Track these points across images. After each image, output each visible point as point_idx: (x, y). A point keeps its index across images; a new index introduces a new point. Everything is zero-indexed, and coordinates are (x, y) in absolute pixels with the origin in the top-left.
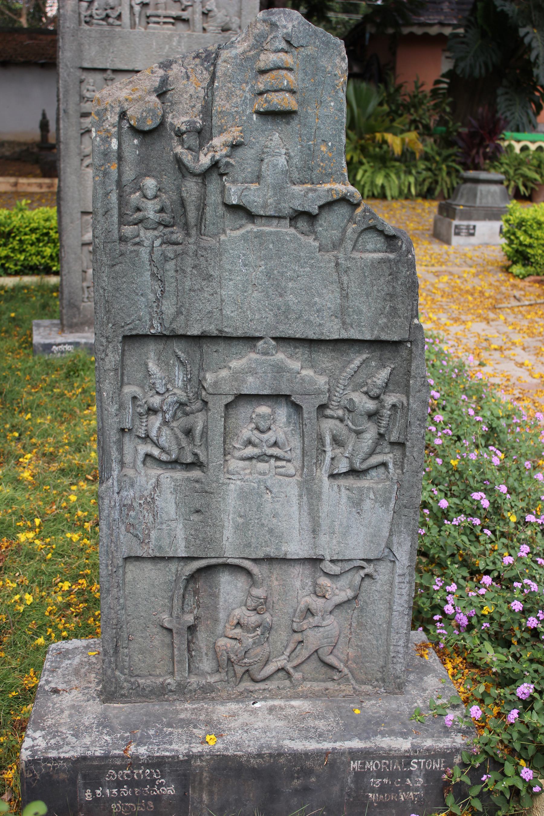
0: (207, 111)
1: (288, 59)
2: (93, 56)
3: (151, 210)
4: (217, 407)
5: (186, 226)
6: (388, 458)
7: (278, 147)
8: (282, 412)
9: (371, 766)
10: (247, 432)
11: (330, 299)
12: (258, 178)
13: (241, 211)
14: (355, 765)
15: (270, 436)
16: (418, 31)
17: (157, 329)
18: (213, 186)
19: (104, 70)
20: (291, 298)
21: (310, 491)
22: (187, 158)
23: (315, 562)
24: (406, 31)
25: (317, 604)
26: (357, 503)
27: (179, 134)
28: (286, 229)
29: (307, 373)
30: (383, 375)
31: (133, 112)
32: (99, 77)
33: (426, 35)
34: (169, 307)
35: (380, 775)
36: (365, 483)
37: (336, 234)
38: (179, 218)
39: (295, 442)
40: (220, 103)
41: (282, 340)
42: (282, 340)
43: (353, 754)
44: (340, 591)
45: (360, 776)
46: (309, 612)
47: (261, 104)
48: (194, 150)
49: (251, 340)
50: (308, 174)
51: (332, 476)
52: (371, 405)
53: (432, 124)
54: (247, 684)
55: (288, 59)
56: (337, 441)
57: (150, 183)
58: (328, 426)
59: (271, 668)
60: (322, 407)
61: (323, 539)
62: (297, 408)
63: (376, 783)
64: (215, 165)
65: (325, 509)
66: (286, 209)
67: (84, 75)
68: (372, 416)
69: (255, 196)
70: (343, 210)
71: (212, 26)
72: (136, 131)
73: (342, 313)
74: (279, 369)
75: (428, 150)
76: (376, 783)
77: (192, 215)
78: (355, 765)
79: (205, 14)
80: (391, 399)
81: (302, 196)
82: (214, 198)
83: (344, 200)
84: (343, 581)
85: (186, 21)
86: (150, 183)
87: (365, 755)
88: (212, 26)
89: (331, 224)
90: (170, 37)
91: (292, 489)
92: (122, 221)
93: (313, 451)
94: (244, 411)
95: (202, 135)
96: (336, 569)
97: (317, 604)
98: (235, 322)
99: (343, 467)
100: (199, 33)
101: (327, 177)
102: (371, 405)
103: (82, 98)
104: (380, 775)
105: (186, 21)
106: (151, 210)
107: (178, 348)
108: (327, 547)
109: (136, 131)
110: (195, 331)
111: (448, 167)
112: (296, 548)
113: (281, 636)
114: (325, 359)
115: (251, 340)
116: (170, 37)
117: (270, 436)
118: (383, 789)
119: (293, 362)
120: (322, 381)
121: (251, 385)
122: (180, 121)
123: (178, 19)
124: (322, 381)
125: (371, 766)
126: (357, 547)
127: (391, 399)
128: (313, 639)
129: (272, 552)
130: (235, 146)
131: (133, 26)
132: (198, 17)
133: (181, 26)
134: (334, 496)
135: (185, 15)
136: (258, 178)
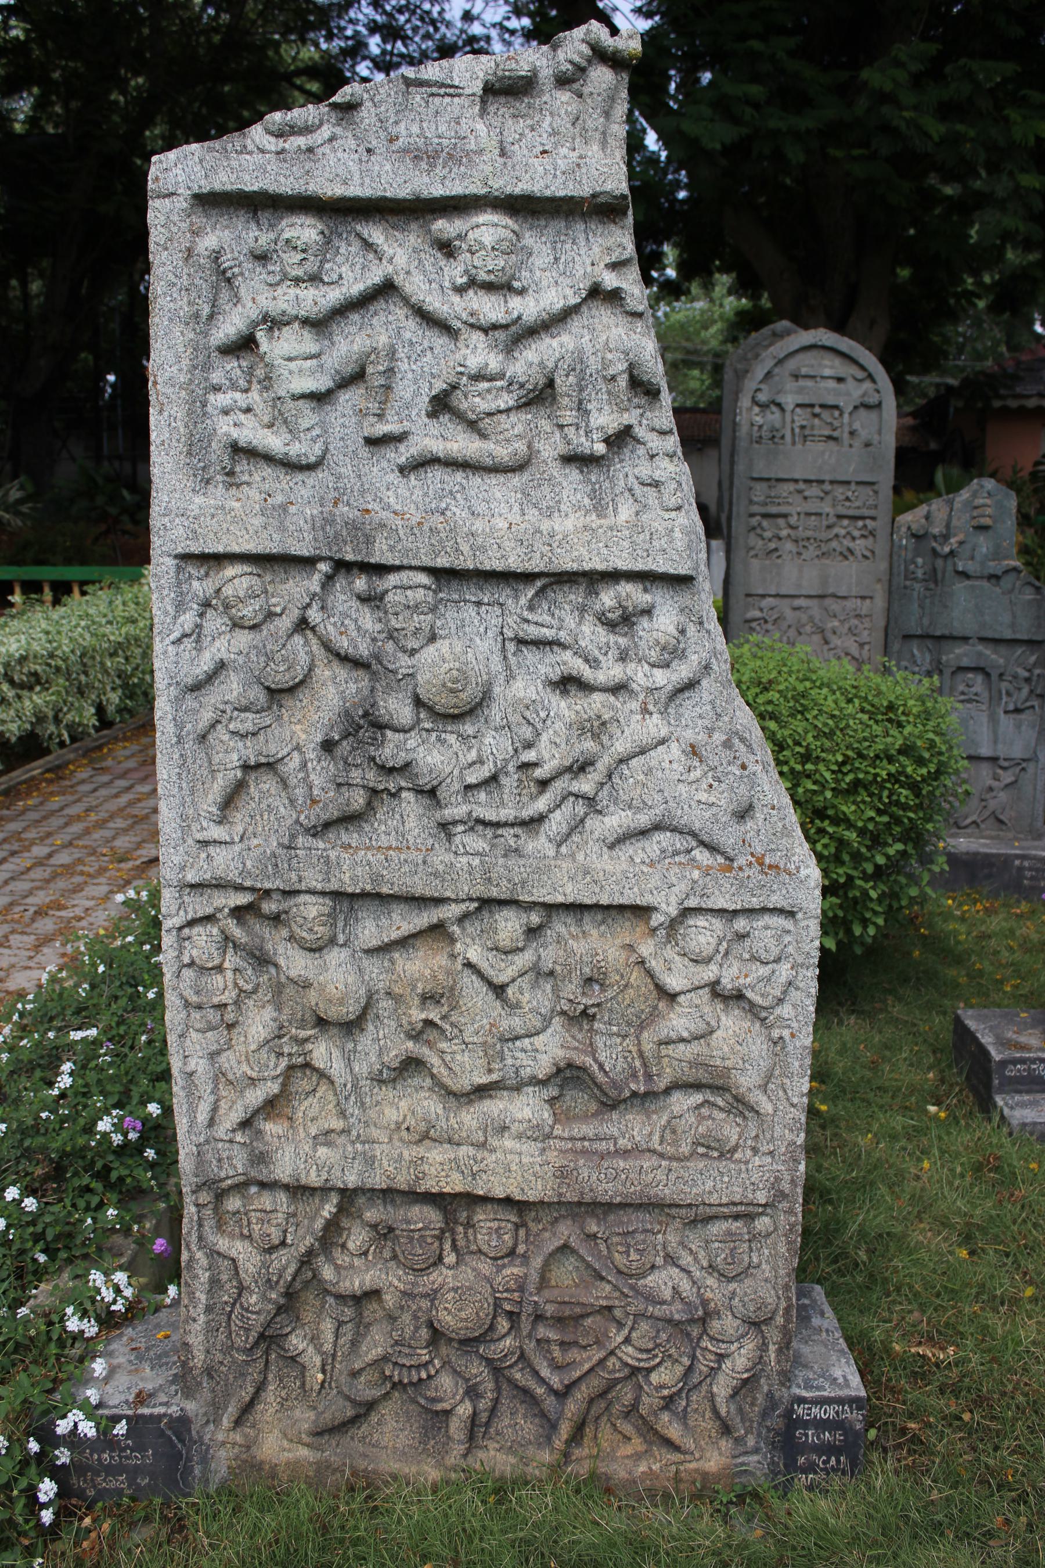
0: (948, 526)
1: (988, 501)
2: (761, 469)
3: (920, 573)
4: (947, 672)
5: (936, 582)
6: (1036, 703)
7: (984, 544)
8: (980, 678)
9: (1026, 864)
10: (961, 687)
11: (1006, 618)
12: (972, 558)
13: (965, 575)
14: (1017, 862)
15: (974, 690)
16: (1013, 404)
17: (919, 632)
18: (949, 562)
19: (768, 480)
20: (987, 618)
21: (993, 720)
22: (938, 548)
23: (994, 760)
24: (997, 404)
25: (995, 784)
26: (1018, 726)
27: (935, 537)
28: (985, 584)
29: (993, 657)
30: (1033, 659)
31: (914, 527)
32: (765, 485)
33: (1022, 409)
34: (926, 621)
35: (1030, 869)
36: (1023, 716)
37: (1009, 586)
38: (933, 577)
39: (986, 694)
40: (955, 522)
41: (982, 639)
42: (982, 639)
43: (1017, 856)
44: (1008, 777)
45: (1021, 869)
46: (991, 789)
47: (975, 523)
48: (942, 545)
49: (965, 639)
50: (997, 555)
51: (1006, 712)
52: (1026, 674)
53: (1032, 513)
54: (954, 830)
55: (988, 501)
56: (1008, 694)
57: (920, 561)
58: (1004, 686)
59: (969, 821)
60: (1001, 675)
61: (1000, 746)
62: (988, 675)
63: (1028, 874)
64: (952, 553)
65: (1001, 729)
66: (986, 573)
67: (752, 484)
68: (1027, 680)
69: (971, 567)
70: (1013, 575)
71: (857, 443)
72: (914, 535)
73: (1013, 625)
74: (980, 654)
75: (1029, 542)
76: (1028, 874)
77: (939, 575)
78: (1017, 862)
79: (852, 433)
80: (1037, 671)
81: (993, 567)
82: (950, 568)
83: (1015, 569)
84: (1010, 772)
85: (835, 439)
86: (920, 561)
87: (1023, 857)
88: (857, 443)
89: (1007, 582)
90: (823, 453)
91: (984, 718)
92: (906, 578)
93: (994, 699)
94: (960, 676)
95: (946, 537)
96: (1006, 764)
97: (995, 784)
98: (958, 630)
99: (1011, 707)
100: (846, 449)
101: (1006, 558)
102: (1026, 674)
103: (751, 502)
104: (1030, 869)
105: (835, 439)
106: (920, 573)
107: (929, 643)
108: (1002, 751)
109: (914, 535)
110: (938, 633)
111: (96, 1043)
112: (985, 751)
113: (974, 802)
114: (1003, 649)
115: (965, 639)
116: (823, 453)
117: (974, 690)
118: (1032, 878)
119: (987, 651)
120: (1001, 661)
121: (965, 662)
122: (936, 531)
123: (830, 438)
124: (1001, 661)
125: (1026, 864)
126: (1017, 752)
127: (1037, 671)
128: (992, 804)
129: (972, 752)
130: (961, 543)
131: (794, 443)
132: (846, 435)
133: (831, 443)
134: (1006, 723)
135: (835, 434)
136: (972, 558)
